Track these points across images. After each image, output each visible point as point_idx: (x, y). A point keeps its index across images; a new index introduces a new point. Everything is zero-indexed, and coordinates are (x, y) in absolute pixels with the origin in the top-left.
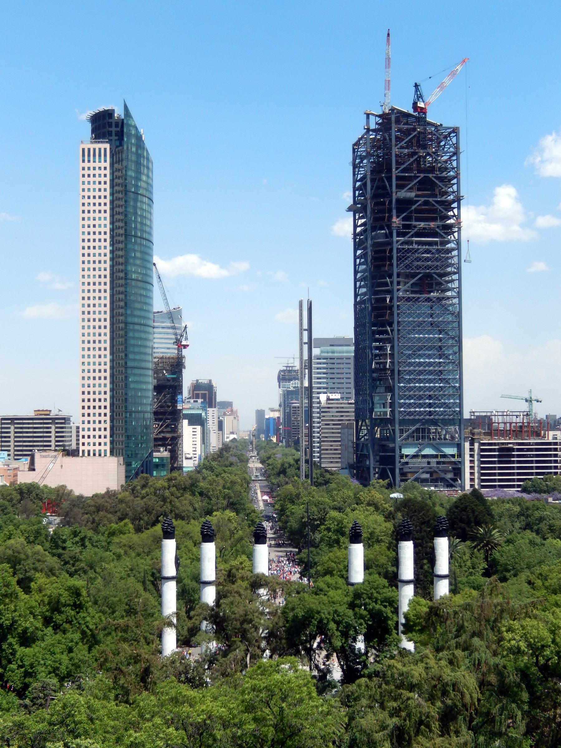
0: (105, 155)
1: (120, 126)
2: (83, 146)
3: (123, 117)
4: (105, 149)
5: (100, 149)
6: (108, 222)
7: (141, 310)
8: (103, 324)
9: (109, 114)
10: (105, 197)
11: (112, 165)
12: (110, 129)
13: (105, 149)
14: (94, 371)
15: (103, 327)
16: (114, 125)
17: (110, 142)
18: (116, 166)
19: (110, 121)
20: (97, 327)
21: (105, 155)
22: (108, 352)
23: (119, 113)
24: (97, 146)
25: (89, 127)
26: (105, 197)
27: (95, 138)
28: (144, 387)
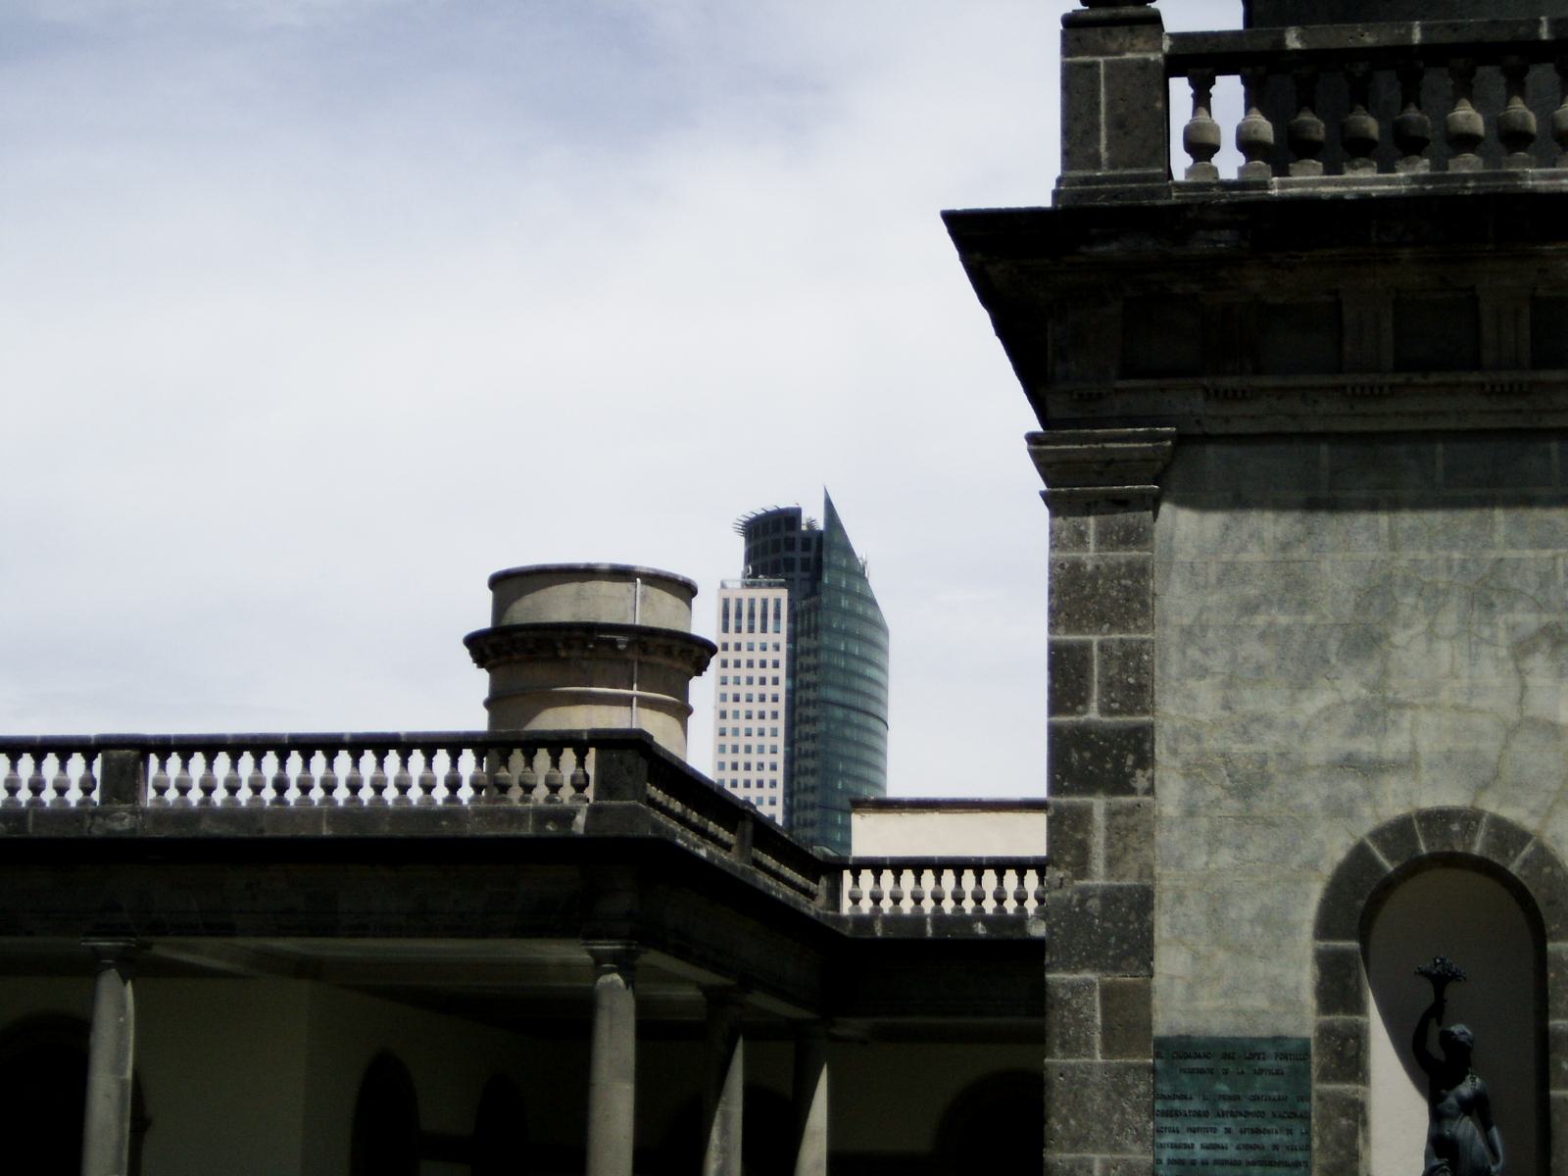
0: (777, 616)
1: (814, 545)
2: (726, 594)
3: (820, 525)
4: (778, 603)
5: (765, 602)
6: (780, 741)
7: (847, 634)
8: (769, 673)
9: (787, 519)
10: (776, 681)
11: (793, 638)
12: (790, 554)
13: (778, 603)
14: (750, 664)
15: (769, 681)
16: (799, 545)
17: (788, 584)
18: (803, 642)
19: (790, 534)
20: (755, 733)
21: (777, 616)
22: (782, 672)
23: (813, 515)
24: (759, 594)
25: (738, 546)
26: (776, 681)
27: (755, 575)
28: (843, 664)
